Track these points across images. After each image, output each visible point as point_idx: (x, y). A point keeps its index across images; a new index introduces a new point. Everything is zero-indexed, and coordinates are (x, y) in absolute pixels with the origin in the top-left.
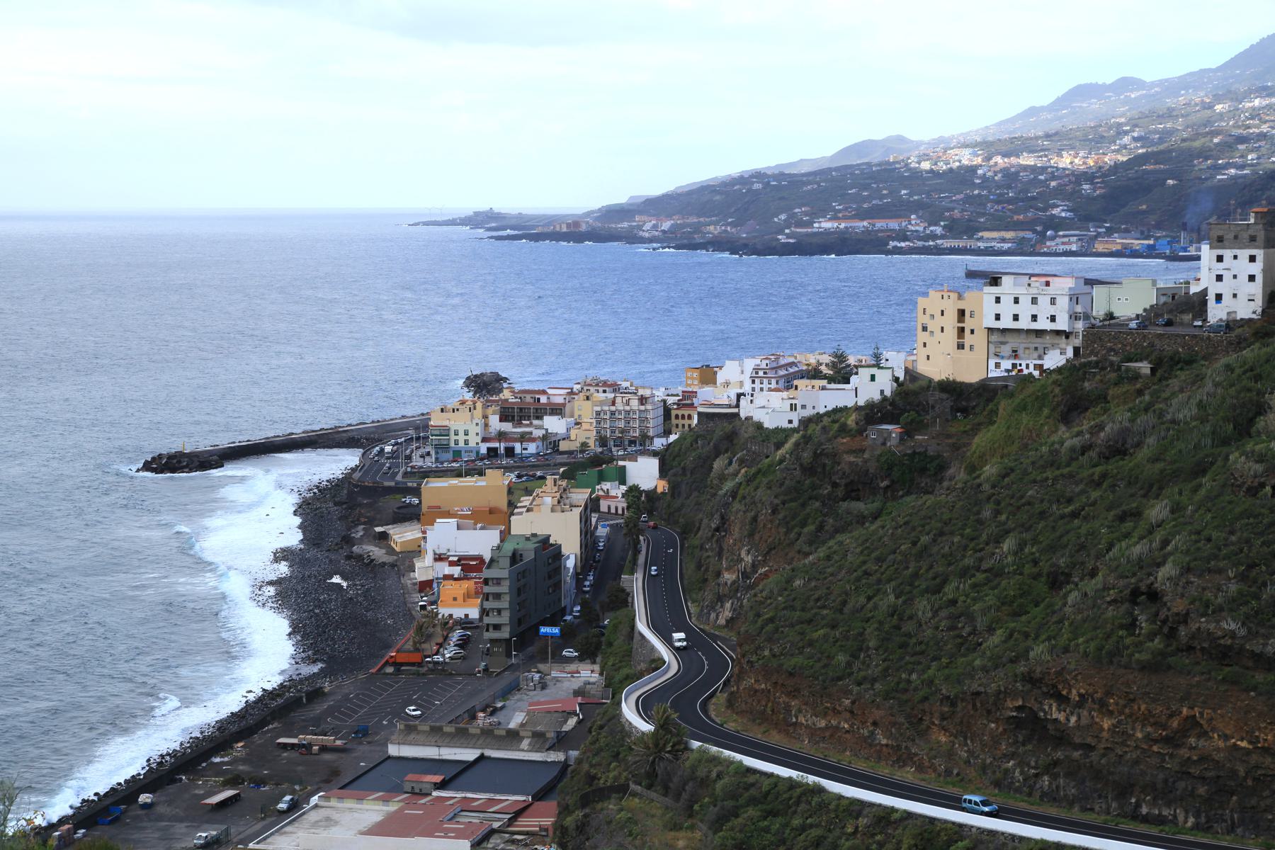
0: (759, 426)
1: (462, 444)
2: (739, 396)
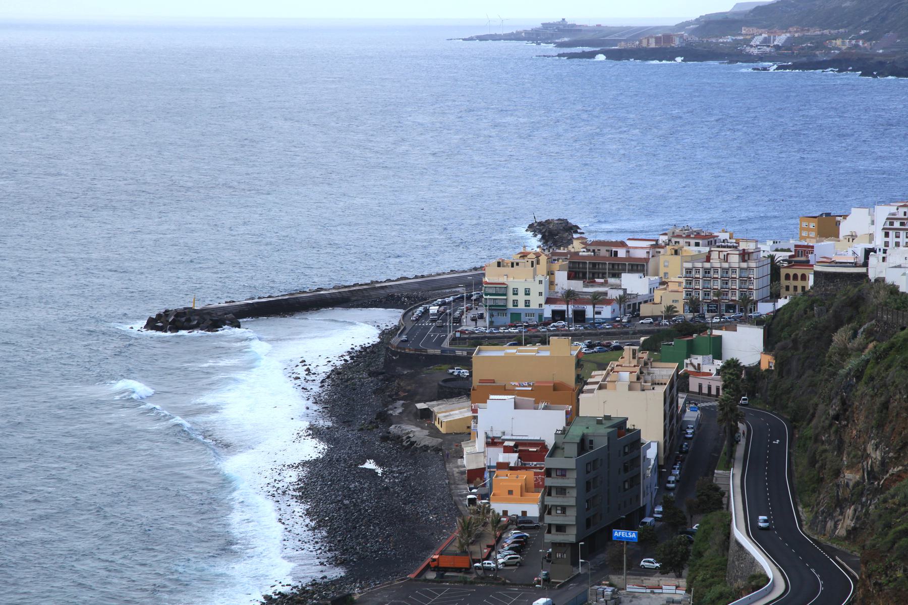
0: (893, 290)
1: (521, 305)
2: (868, 252)
